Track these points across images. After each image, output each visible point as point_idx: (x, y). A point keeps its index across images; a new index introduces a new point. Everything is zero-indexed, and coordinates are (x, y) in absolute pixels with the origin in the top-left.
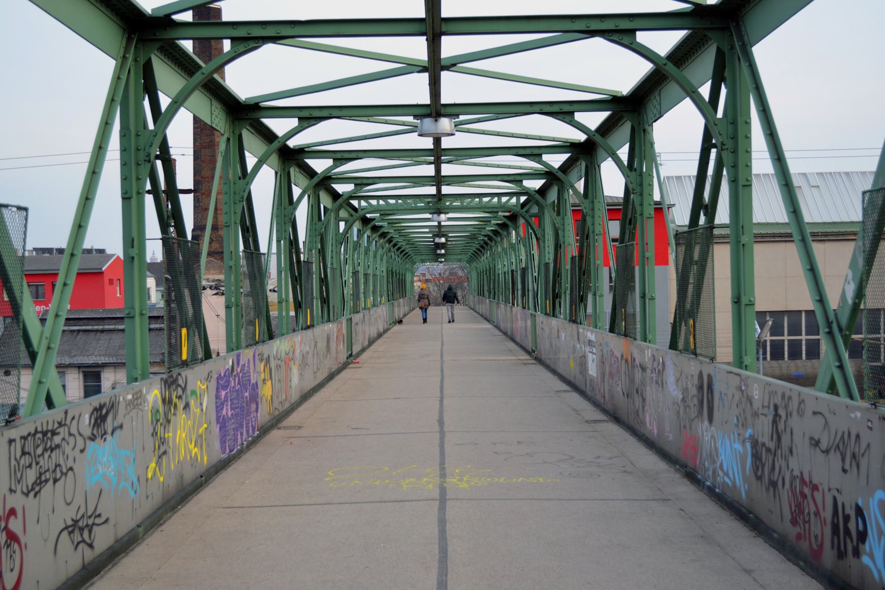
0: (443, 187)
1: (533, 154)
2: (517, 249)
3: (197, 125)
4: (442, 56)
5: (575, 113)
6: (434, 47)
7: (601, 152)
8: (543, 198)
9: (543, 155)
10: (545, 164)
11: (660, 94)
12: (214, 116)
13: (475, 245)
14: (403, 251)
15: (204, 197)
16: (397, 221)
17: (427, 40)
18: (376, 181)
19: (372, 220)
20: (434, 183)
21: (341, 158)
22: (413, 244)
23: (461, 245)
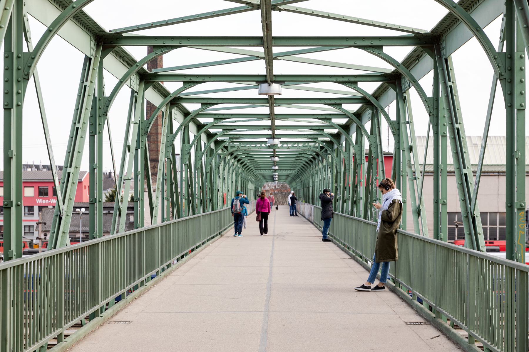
0: (276, 121)
3: (148, 106)
5: (384, 47)
6: (268, 50)
7: (406, 82)
10: (360, 91)
13: (307, 156)
15: (151, 144)
16: (238, 136)
18: (229, 116)
19: (215, 134)
20: (268, 105)
23: (292, 161)
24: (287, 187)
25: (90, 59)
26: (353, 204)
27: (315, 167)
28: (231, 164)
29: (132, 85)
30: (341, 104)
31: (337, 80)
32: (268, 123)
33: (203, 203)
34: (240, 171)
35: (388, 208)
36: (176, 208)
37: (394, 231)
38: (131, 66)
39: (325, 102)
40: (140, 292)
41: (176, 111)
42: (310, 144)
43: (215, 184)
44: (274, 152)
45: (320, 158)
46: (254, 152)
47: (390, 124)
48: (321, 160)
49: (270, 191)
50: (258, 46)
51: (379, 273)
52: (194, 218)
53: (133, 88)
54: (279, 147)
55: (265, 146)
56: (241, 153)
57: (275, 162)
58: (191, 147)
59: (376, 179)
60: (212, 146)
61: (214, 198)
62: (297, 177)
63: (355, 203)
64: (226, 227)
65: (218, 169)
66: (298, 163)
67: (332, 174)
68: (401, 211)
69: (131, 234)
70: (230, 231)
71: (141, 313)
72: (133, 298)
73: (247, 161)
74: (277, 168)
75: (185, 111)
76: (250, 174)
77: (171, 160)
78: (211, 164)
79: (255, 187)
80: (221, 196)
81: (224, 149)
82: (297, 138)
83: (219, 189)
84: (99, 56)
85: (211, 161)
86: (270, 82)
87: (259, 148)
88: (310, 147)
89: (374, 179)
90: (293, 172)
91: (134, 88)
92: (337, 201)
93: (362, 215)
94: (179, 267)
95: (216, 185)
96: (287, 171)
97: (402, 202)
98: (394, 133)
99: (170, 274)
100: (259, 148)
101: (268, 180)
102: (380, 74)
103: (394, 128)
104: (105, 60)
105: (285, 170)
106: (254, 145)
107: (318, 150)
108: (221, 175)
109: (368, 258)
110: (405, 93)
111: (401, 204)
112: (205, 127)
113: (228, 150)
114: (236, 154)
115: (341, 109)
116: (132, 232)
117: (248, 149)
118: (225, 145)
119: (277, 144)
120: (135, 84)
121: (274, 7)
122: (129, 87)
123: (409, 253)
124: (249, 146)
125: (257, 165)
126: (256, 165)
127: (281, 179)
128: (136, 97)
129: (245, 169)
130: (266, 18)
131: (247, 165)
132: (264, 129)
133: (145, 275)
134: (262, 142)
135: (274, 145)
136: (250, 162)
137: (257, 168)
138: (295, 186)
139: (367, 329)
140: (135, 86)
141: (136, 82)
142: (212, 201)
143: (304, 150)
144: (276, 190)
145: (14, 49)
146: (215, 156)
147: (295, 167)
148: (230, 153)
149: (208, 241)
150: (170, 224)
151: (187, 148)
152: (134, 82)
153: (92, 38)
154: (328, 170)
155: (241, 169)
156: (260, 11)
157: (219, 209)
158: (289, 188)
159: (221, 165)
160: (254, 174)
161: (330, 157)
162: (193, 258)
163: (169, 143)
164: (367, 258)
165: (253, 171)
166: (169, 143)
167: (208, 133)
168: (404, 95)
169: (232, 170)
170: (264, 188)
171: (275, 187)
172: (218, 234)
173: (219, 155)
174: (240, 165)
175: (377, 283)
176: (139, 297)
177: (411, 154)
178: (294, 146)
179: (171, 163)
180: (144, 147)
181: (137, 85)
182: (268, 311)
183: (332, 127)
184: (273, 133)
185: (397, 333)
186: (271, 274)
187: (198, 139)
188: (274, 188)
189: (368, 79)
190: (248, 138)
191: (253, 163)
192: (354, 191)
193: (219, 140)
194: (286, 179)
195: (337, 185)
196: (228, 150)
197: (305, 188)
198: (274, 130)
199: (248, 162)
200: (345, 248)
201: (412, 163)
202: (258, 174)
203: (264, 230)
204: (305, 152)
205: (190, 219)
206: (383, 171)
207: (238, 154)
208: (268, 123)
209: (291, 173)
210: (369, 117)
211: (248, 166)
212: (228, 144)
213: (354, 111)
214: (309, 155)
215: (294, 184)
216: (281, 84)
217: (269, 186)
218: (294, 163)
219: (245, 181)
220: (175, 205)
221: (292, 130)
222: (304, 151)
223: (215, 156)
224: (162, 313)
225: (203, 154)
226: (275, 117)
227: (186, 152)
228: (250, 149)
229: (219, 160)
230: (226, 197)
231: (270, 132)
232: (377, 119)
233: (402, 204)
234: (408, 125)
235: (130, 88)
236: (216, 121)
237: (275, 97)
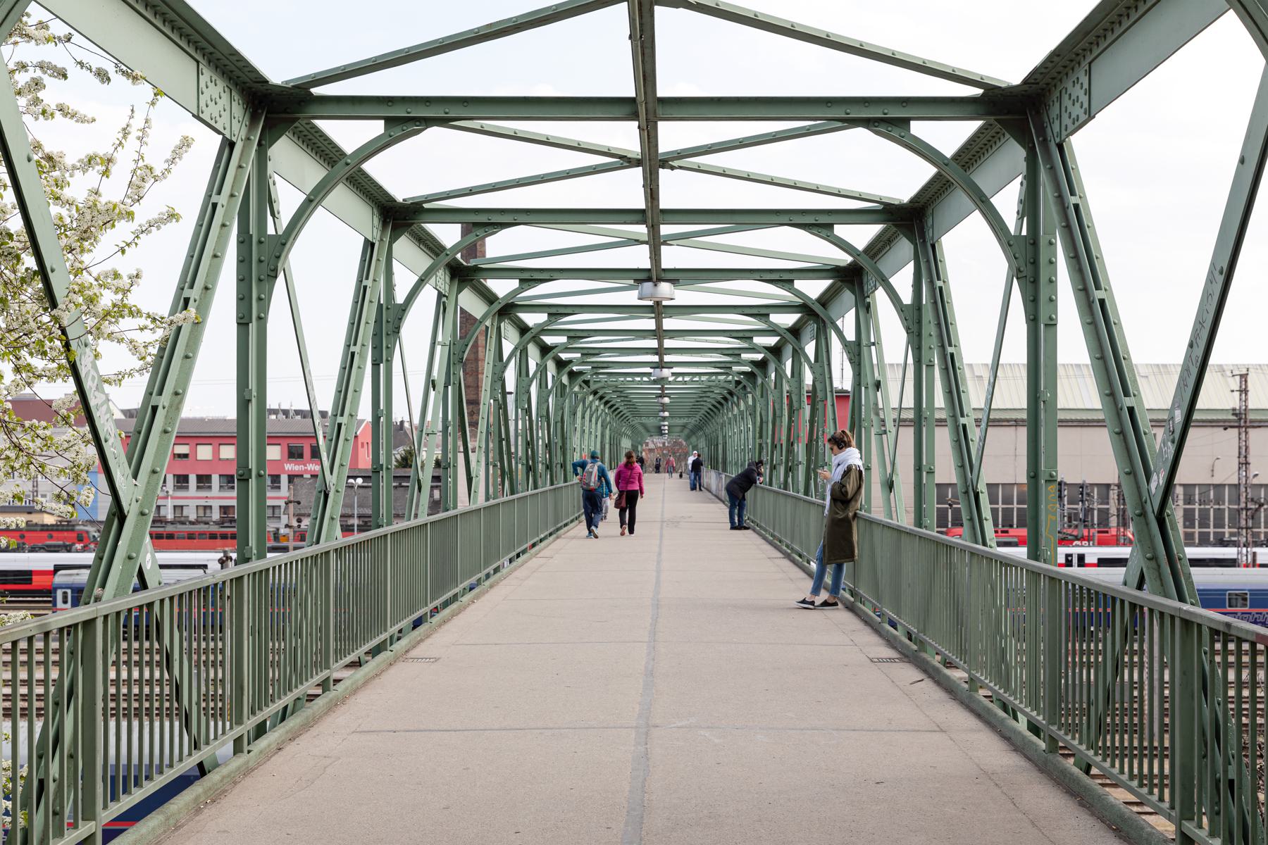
1: (783, 278)
4: (662, 234)
5: (912, 122)
6: (649, 136)
7: (870, 280)
8: (797, 338)
10: (798, 294)
11: (1089, 73)
14: (612, 406)
16: (605, 365)
17: (639, 127)
18: (592, 334)
19: (570, 362)
20: (653, 315)
21: (530, 278)
22: (626, 397)
25: (232, 145)
29: (439, 284)
32: (653, 344)
34: (608, 419)
37: (851, 514)
38: (437, 255)
43: (568, 440)
44: (662, 389)
57: (663, 405)
58: (532, 381)
59: (823, 432)
60: (565, 379)
67: (754, 424)
74: (667, 414)
78: (563, 409)
79: (632, 445)
81: (583, 385)
84: (256, 139)
87: (639, 382)
89: (820, 433)
90: (693, 421)
97: (862, 469)
102: (829, 267)
104: (395, 246)
106: (630, 379)
107: (731, 387)
108: (578, 425)
112: (554, 351)
115: (767, 321)
122: (194, 115)
124: (622, 379)
128: (444, 303)
129: (616, 416)
130: (651, 181)
131: (619, 411)
132: (647, 353)
143: (710, 387)
145: (253, 230)
151: (524, 384)
168: (868, 300)
173: (576, 394)
175: (824, 596)
177: (879, 394)
182: (654, 641)
189: (811, 275)
201: (881, 406)
208: (653, 344)
214: (717, 394)
215: (693, 439)
227: (523, 391)
231: (656, 358)
234: (873, 348)
236: (571, 341)
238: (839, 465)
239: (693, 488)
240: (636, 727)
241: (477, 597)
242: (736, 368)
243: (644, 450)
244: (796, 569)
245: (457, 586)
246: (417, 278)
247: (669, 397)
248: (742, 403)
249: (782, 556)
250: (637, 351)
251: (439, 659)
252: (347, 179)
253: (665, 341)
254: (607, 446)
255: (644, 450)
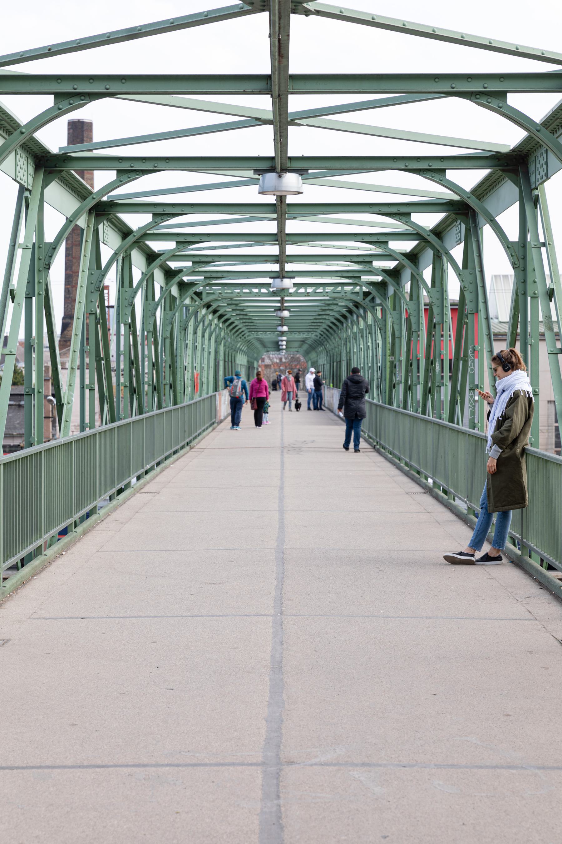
2: (373, 331)
5: (447, 171)
9: (509, 95)
12: (18, 168)
13: (338, 309)
18: (204, 238)
19: (179, 271)
20: (275, 216)
24: (300, 361)
26: (426, 394)
27: (351, 327)
28: (206, 323)
29: (20, 175)
30: (409, 214)
31: (406, 166)
32: (274, 250)
33: (158, 393)
34: (222, 334)
35: (506, 408)
36: (107, 404)
37: (518, 450)
38: (9, 133)
39: (380, 211)
40: (33, 569)
41: (107, 228)
42: (345, 287)
43: (179, 358)
44: (282, 301)
45: (362, 311)
46: (247, 302)
47: (508, 248)
48: (363, 315)
49: (272, 366)
50: (260, 93)
51: (492, 532)
52: (141, 419)
53: (20, 181)
54: (291, 293)
55: (267, 292)
56: (224, 303)
57: (282, 319)
58: (136, 293)
59: (474, 350)
60: (175, 291)
61: (178, 382)
62: (319, 344)
63: (430, 392)
64: (198, 432)
65: (184, 331)
66: (321, 321)
67: (384, 339)
68: (531, 412)
69: (14, 459)
70: (206, 438)
71: (29, 618)
72: (19, 583)
73: (235, 318)
74: (285, 328)
75: (123, 228)
76: (239, 339)
77: (98, 317)
78: (172, 323)
79: (248, 362)
80: (189, 378)
81: (196, 297)
82: (323, 277)
83: (186, 367)
85: (173, 318)
86: (281, 169)
87: (257, 295)
88: (345, 293)
89: (470, 351)
90: (313, 336)
91: (23, 182)
92: (394, 387)
93: (446, 414)
94: (111, 513)
95: (180, 359)
96: (293, 334)
97: (531, 395)
98: (515, 264)
99: (94, 527)
100: (256, 294)
101: (269, 349)
102: (444, 201)
103: (515, 256)
104: (46, 191)
105: (299, 332)
106: (247, 291)
107: (359, 299)
108: (190, 341)
109: (461, 495)
110: (537, 189)
111: (531, 398)
112: (161, 258)
113: (201, 300)
114: (217, 305)
115: (408, 222)
116: (15, 457)
117: (237, 297)
118: (197, 290)
119: (289, 288)
120: (26, 174)
121: (295, 6)
122: (13, 179)
123: (552, 494)
124: (238, 291)
125: (252, 324)
126: (250, 324)
127: (291, 348)
128: (26, 198)
129: (231, 331)
130: (280, 28)
131: (234, 325)
132: (266, 261)
133: (44, 534)
134: (261, 285)
135: (283, 289)
136: (240, 319)
137: (251, 330)
138: (315, 359)
139: (486, 658)
140: (25, 178)
141: (26, 169)
142: (174, 388)
143: (334, 299)
144: (283, 365)
146: (179, 308)
147: (316, 327)
148: (206, 304)
149: (166, 458)
150: (96, 434)
151: (127, 296)
152: (23, 170)
153: (30, 161)
154: (375, 333)
155: (224, 331)
156: (266, 14)
157: (187, 402)
158: (305, 361)
159: (189, 324)
160: (247, 338)
161: (380, 310)
162: (138, 492)
163: (93, 285)
164: (459, 494)
165: (245, 334)
166: (93, 285)
167: (166, 269)
168: (536, 192)
169: (209, 332)
170: (262, 362)
171: (281, 359)
172: (185, 445)
173: (187, 307)
174: (222, 325)
175: (486, 548)
176: (30, 580)
177: (552, 304)
178: (318, 291)
179: (97, 323)
180: (44, 293)
181: (29, 176)
182: (281, 614)
183: (390, 256)
184: (282, 269)
185: (548, 668)
186: (282, 528)
187: (149, 279)
188: (278, 361)
189: (466, 163)
190: (237, 278)
191: (244, 321)
192: (428, 370)
193: (186, 281)
194: (300, 347)
195: (395, 358)
196: (201, 300)
197: (333, 363)
198: (283, 263)
199: (236, 319)
200: (394, 459)
201: (554, 318)
202: (252, 339)
203: (258, 422)
204: (335, 302)
205: (133, 422)
206: (489, 336)
207: (219, 306)
208: (274, 250)
209: (310, 338)
210: (458, 238)
211: (236, 326)
212: (202, 288)
213: (429, 227)
214: (342, 305)
215: (313, 355)
216: (302, 175)
217: (271, 358)
218: (315, 321)
219: (231, 352)
220: (105, 398)
221: (314, 263)
222: (334, 300)
223: (179, 308)
224: (71, 620)
225: (158, 305)
226: (287, 238)
227: (126, 303)
228: (241, 297)
229: (187, 316)
230: (199, 381)
231: (276, 267)
232: (475, 240)
233: (533, 398)
234: (543, 250)
235: (16, 180)
236: (181, 247)
237: (290, 200)
238: (504, 391)
239: (316, 408)
240: (263, 764)
241: (67, 548)
242: (365, 278)
243: (259, 366)
244: (441, 509)
245: (41, 537)
246: (113, 252)
247: (289, 310)
248: (369, 315)
249: (423, 491)
250: (255, 258)
251: (8, 640)
252: (20, 146)
253: (287, 247)
254: (221, 363)
255: (259, 366)
